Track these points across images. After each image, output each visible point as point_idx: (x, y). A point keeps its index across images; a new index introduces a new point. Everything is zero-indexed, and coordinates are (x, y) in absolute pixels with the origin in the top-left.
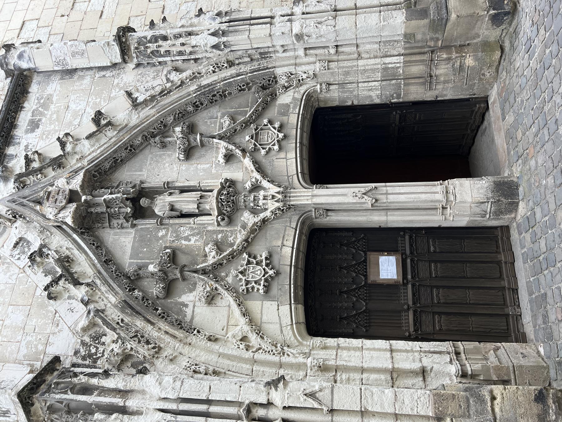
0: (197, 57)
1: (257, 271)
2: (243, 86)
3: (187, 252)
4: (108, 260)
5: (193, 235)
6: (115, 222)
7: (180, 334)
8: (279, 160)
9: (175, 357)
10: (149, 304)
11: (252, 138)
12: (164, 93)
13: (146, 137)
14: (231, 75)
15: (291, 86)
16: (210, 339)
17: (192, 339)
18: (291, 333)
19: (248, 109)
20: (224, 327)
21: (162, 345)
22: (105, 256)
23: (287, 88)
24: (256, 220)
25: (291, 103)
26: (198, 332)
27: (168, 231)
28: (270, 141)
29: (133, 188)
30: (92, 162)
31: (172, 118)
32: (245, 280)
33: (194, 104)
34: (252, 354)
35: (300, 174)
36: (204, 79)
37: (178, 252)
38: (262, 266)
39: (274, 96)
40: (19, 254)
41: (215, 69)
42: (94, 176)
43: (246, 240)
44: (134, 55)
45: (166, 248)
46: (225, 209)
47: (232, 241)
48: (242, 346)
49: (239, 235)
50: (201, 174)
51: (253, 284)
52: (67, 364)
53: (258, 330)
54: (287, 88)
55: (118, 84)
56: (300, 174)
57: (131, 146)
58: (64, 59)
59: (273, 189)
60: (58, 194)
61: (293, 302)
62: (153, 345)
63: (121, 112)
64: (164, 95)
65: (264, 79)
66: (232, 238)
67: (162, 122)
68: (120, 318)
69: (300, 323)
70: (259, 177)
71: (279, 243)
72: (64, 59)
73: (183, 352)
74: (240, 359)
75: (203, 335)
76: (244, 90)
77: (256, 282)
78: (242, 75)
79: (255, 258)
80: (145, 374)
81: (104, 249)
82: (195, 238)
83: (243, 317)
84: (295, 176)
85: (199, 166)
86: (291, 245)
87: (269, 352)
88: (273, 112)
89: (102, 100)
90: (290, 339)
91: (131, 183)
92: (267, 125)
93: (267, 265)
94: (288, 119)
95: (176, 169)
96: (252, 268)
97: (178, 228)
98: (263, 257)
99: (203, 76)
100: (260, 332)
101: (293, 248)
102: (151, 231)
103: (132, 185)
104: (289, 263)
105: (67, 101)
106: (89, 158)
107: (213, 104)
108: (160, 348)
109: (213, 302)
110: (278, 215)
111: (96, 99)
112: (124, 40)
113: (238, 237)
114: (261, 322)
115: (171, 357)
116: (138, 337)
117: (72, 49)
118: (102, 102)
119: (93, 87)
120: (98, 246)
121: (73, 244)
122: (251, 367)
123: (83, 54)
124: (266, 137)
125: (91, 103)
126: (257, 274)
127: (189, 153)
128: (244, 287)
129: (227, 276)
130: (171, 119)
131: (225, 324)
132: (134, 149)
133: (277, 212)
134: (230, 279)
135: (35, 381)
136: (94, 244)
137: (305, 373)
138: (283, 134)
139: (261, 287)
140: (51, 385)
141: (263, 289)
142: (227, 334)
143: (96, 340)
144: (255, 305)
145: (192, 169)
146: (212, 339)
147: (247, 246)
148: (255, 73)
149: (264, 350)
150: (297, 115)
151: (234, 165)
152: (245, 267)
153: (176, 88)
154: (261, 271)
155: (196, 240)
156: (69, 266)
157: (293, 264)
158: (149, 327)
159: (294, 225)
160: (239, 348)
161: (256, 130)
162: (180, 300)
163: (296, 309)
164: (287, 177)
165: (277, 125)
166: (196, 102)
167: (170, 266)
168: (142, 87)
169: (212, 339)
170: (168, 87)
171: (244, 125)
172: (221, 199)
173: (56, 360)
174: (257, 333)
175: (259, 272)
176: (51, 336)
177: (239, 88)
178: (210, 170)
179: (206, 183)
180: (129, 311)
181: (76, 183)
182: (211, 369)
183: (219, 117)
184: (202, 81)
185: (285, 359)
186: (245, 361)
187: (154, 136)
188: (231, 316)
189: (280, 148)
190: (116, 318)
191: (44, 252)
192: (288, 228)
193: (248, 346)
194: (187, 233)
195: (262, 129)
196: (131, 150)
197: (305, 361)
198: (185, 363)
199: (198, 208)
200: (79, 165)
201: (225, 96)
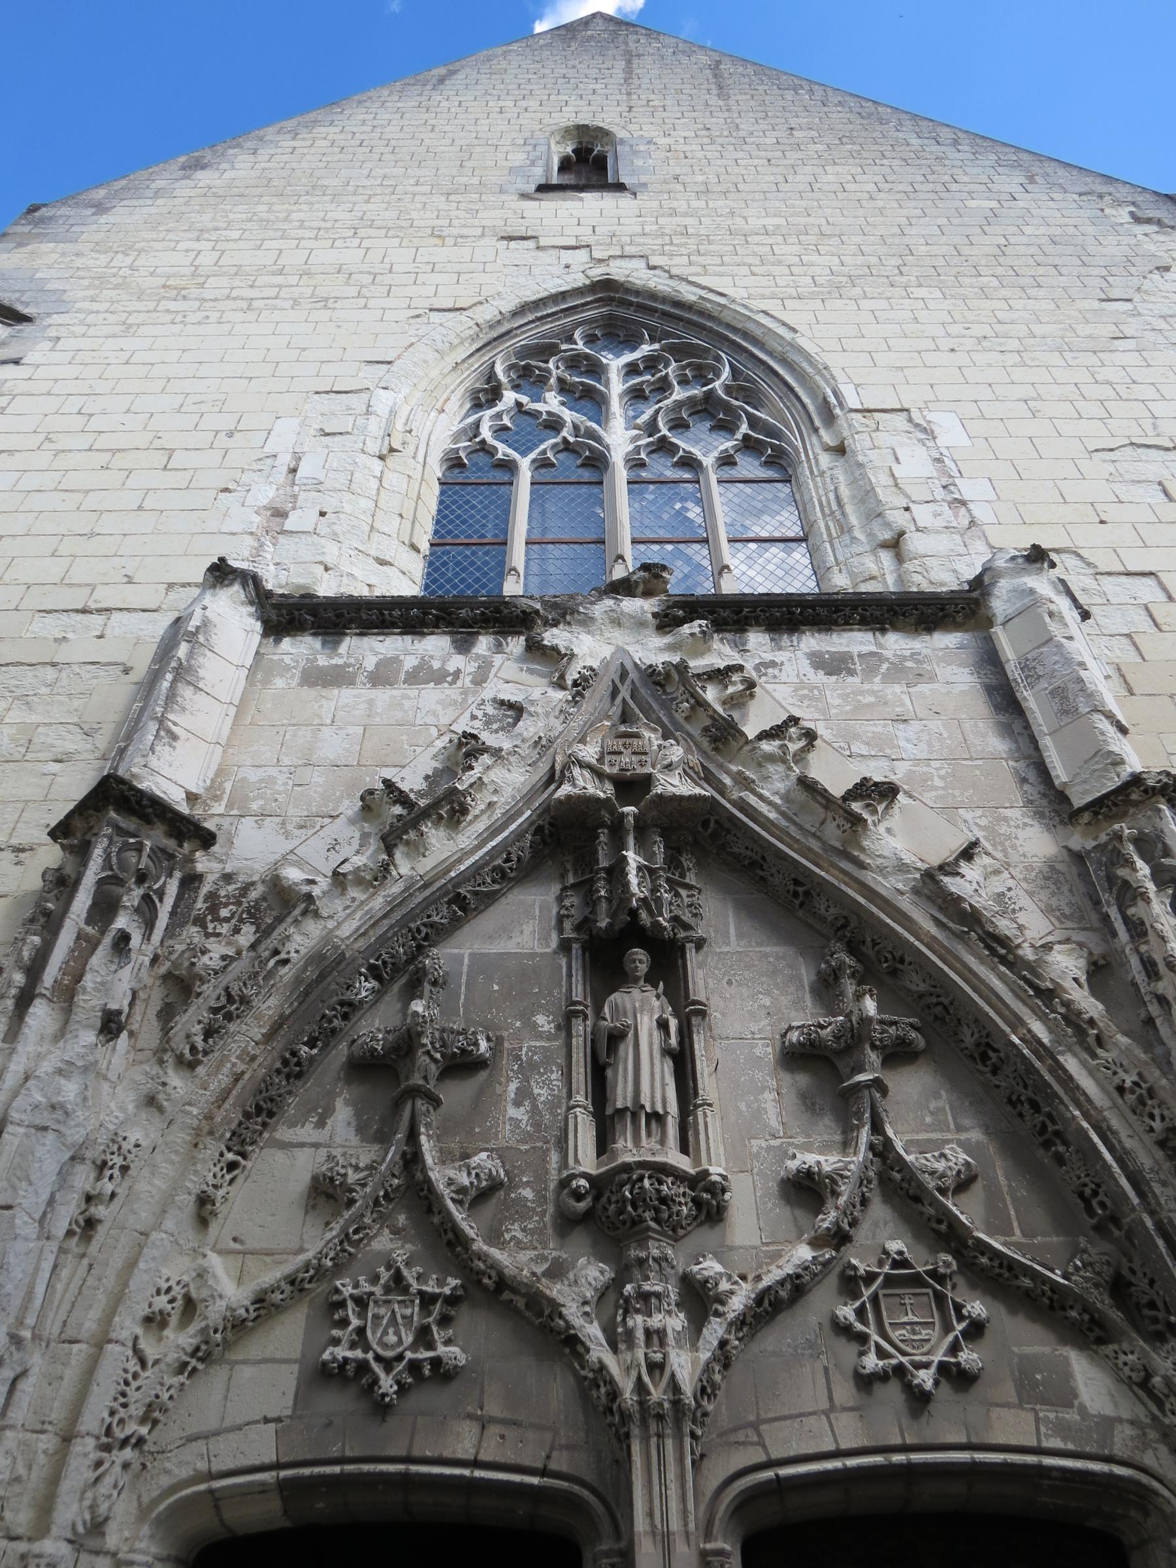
0: (1158, 1022)
1: (397, 1333)
2: (1102, 1205)
3: (483, 1104)
4: (462, 900)
5: (534, 1111)
6: (573, 900)
7: (230, 1114)
8: (822, 1381)
9: (160, 1109)
10: (330, 1022)
11: (896, 1264)
12: (999, 948)
13: (844, 927)
14: (1126, 1152)
15: (1160, 1404)
16: (204, 1200)
17: (212, 1148)
18: (184, 1473)
19: (1018, 1236)
20: (242, 1243)
21: (201, 1070)
22: (476, 893)
23: (1145, 1384)
24: (572, 1312)
25: (1082, 1410)
26: (232, 1166)
27: (549, 1037)
28: (895, 1335)
29: (675, 919)
30: (741, 810)
31: (922, 987)
32: (372, 1294)
33: (988, 1045)
34: (125, 1335)
35: (769, 1474)
36: (1084, 1064)
37: (483, 1075)
38: (414, 1347)
39: (1091, 1334)
40: (485, 715)
41: (1132, 1092)
42: (705, 824)
43: (503, 1283)
44: (1103, 838)
45: (497, 1044)
46: (614, 1199)
47: (507, 1236)
48: (161, 1302)
49: (525, 1256)
50: (743, 1106)
51: (355, 1322)
52: (203, 863)
53: (209, 1354)
54: (1145, 1384)
55: (1006, 819)
56: (769, 1474)
57: (807, 893)
58: (1039, 677)
59: (685, 1365)
60: (634, 753)
61: (283, 1474)
62: (200, 1045)
63: (900, 842)
64: (988, 947)
65: (1152, 1282)
66: (519, 1235)
67: (902, 961)
68: (293, 954)
69: (217, 1508)
70: (737, 1304)
71: (493, 1408)
72: (1039, 677)
73: (174, 1127)
74: (117, 1300)
75: (218, 1181)
76: (1090, 1211)
77: (361, 1331)
78: (1141, 1194)
79: (445, 1321)
80: (101, 1031)
81: (497, 887)
82: (525, 1118)
83: (252, 1297)
84: (759, 1457)
85: (769, 1097)
86: (484, 1457)
87: (124, 1395)
88: (1027, 1339)
89: (940, 792)
90: (167, 1472)
91: (695, 915)
92: (961, 1318)
93: (414, 1367)
94: (1008, 1405)
95: (755, 1028)
96: (408, 1312)
97: (558, 1065)
98: (441, 1350)
99: (1094, 1056)
100: (204, 1355)
101: (476, 1464)
102: (551, 994)
103: (687, 917)
104: (416, 1453)
105: (920, 715)
106: (752, 800)
107: (1009, 1109)
108: (192, 1066)
109: (321, 1200)
110: (594, 1393)
111: (941, 778)
112: (1134, 797)
113: (516, 1257)
114: (237, 1362)
115: (161, 1096)
116: (232, 1006)
117: (1071, 686)
118: (934, 793)
119: (980, 762)
120: (505, 873)
121: (503, 814)
122: (84, 1335)
123: (1066, 712)
124: (911, 1318)
125: (926, 769)
126: (385, 1333)
127: (801, 1056)
128: (348, 1291)
129: (396, 1231)
130: (916, 983)
131: (251, 1244)
132: (802, 905)
133: (603, 1390)
134: (383, 1242)
135: (145, 802)
136: (508, 860)
137: (20, 1531)
138: (929, 1385)
139: (342, 1352)
140: (134, 836)
141: (334, 1360)
142: (220, 1252)
143: (249, 913)
144: (289, 1335)
145: (759, 1075)
146: (204, 1209)
147: (485, 1288)
148: (1160, 1243)
149: (135, 1376)
150: (1033, 1443)
151: (781, 1212)
152: (413, 1290)
153: (1024, 979)
154: (393, 1347)
155: (516, 1122)
156: (441, 817)
157: (414, 1468)
158: (257, 1033)
159: (559, 1463)
160: (158, 1292)
161: (933, 1274)
162: (339, 1103)
163: (262, 1489)
164: (752, 1418)
165: (968, 1357)
166: (995, 1050)
167: (435, 1061)
168: (1011, 883)
169: (204, 1209)
170: (1020, 952)
171: (943, 1227)
172: (641, 1179)
173: (207, 839)
174: (197, 1349)
175: (392, 1338)
176: (278, 819)
177: (1088, 1191)
178: (750, 1127)
179: (713, 1128)
180: (311, 974)
181: (675, 785)
182: (99, 1211)
183: (963, 1136)
184: (1075, 1055)
185: (85, 1448)
186: (107, 1321)
187: (853, 949)
188: (268, 1259)
189: (865, 1382)
190: (291, 947)
191: (477, 759)
192: (548, 1436)
193: (163, 1324)
194: (542, 1093)
195: (940, 1298)
196: (796, 894)
197: (54, 1531)
198: (135, 1135)
199: (621, 1112)
200: (728, 781)
201: (1047, 1144)
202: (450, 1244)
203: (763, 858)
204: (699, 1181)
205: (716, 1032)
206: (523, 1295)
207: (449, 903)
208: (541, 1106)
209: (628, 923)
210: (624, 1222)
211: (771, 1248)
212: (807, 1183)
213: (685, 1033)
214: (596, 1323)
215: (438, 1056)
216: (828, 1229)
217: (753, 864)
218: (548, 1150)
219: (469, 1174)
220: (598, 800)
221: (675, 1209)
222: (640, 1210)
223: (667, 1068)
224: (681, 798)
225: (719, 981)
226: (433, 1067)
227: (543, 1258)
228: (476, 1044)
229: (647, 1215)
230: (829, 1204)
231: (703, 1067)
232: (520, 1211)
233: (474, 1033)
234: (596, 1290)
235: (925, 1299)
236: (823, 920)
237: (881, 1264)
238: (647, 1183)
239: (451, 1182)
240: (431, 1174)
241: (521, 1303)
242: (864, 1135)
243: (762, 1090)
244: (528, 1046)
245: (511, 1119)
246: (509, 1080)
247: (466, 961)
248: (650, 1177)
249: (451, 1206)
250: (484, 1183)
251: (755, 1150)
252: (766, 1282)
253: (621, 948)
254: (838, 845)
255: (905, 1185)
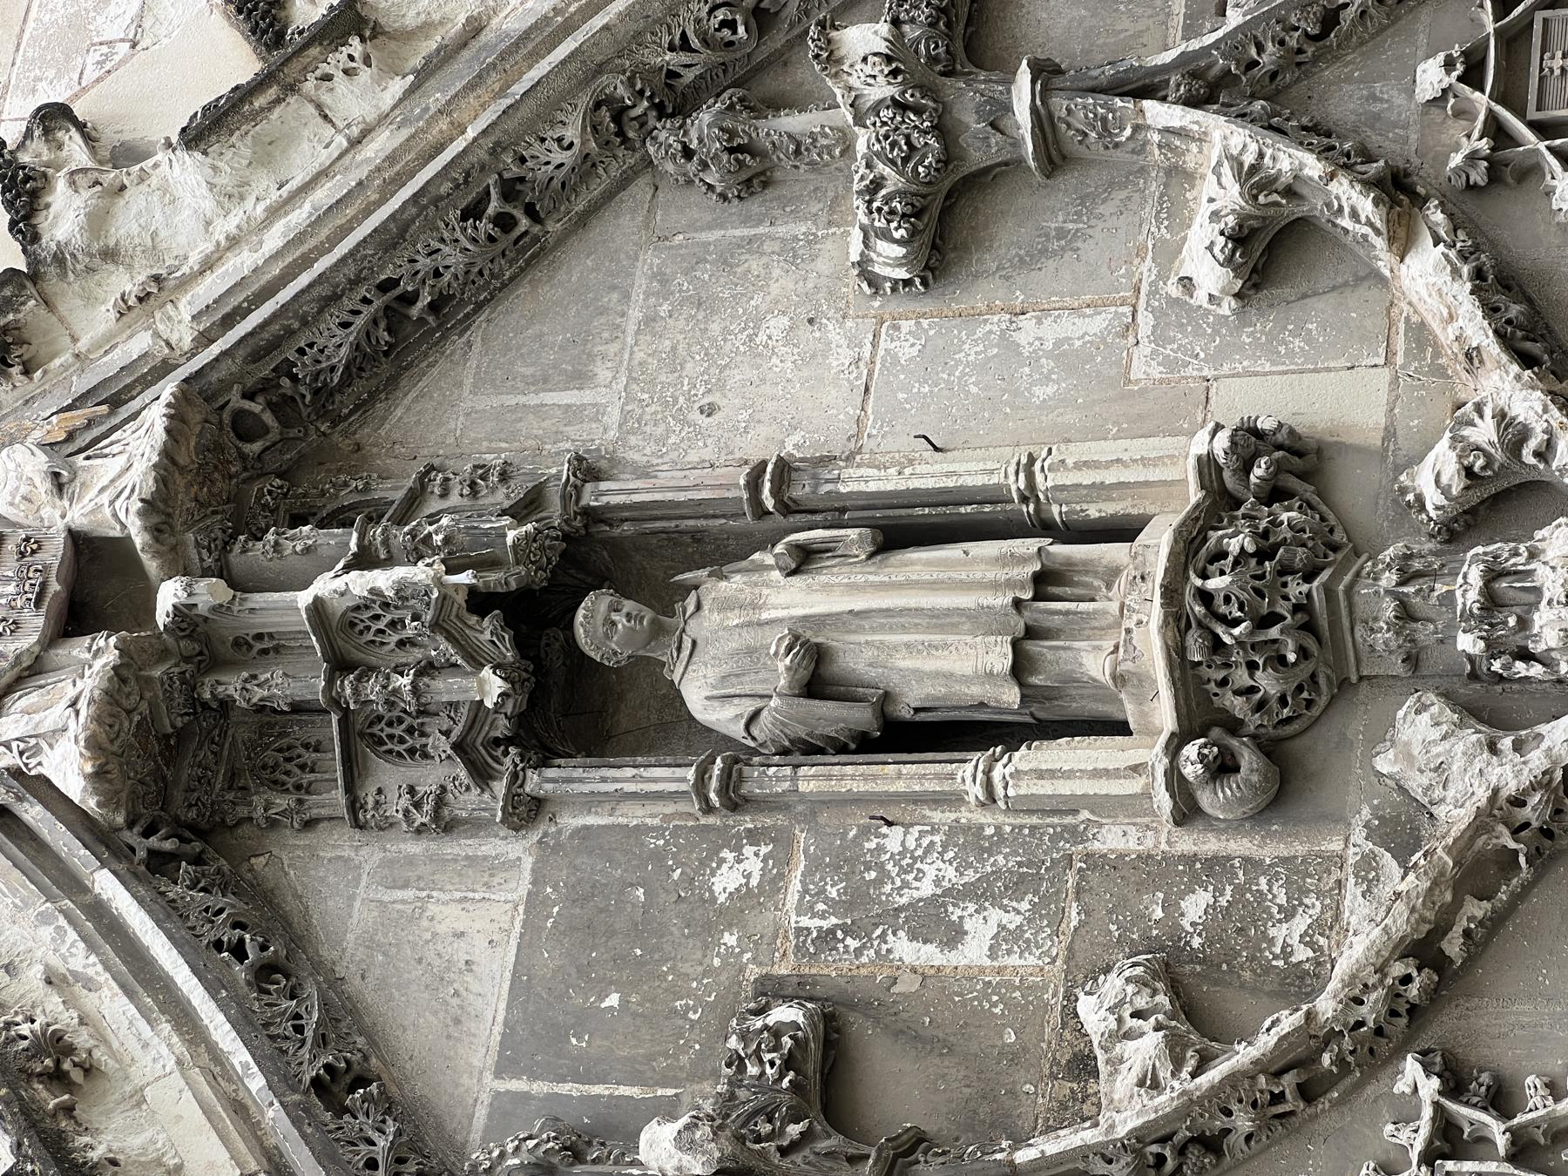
5: (980, 894)
11: (1474, 76)
13: (619, 115)
22: (322, 1041)
27: (783, 844)
30: (228, 321)
37: (859, 1027)
42: (244, 427)
43: (1422, 949)
45: (771, 991)
46: (1241, 677)
47: (1302, 954)
57: (510, 189)
66: (1301, 923)
81: (311, 990)
82: (995, 915)
85: (1028, 331)
91: (504, 477)
95: (845, 356)
97: (865, 832)
106: (209, 288)
113: (1361, 925)
120: (269, 961)
121: (91, 947)
132: (530, 211)
145: (971, 351)
155: (1005, 938)
156: (68, 1110)
167: (806, 1137)
172: (1205, 597)
179: (1079, 470)
200: (139, 344)
202: (1307, 1093)
203: (386, 286)
204: (1220, 501)
205: (838, 447)
206: (1457, 904)
207: (341, 1110)
208: (970, 876)
209: (509, 622)
210: (1303, 653)
211: (1400, 344)
212: (1259, 248)
213: (838, 512)
214: (1543, 729)
215: (794, 1130)
216: (1376, 203)
217: (396, 311)
218: (1088, 856)
219: (1129, 1035)
220: (119, 673)
221: (1285, 532)
222: (1283, 608)
223: (919, 561)
224: (167, 454)
225: (699, 433)
226: (823, 1145)
227: (1367, 865)
228: (776, 1032)
229: (1296, 588)
230: (1314, 205)
231: (930, 475)
232: (1242, 919)
233: (744, 1037)
234: (1461, 725)
235: (1556, 28)
236: (587, 166)
237: (1464, 113)
238: (1215, 583)
239: (1149, 1082)
240: (1121, 1132)
241: (1476, 909)
242: (1159, 114)
243: (1008, 344)
244: (795, 912)
245: (993, 952)
246: (883, 957)
247: (518, 1085)
248: (1204, 576)
249: (1214, 1074)
250: (1162, 999)
251: (1156, 371)
252: (1479, 332)
253: (570, 640)
254: (398, 86)
255: (1293, 41)
